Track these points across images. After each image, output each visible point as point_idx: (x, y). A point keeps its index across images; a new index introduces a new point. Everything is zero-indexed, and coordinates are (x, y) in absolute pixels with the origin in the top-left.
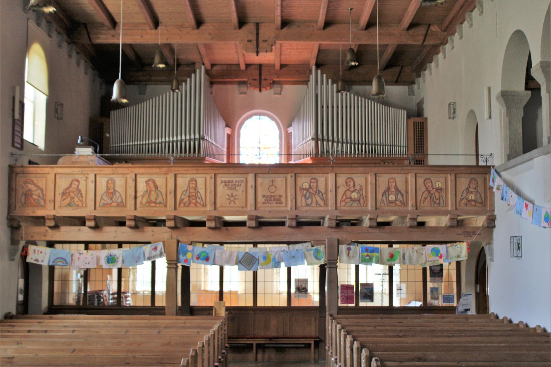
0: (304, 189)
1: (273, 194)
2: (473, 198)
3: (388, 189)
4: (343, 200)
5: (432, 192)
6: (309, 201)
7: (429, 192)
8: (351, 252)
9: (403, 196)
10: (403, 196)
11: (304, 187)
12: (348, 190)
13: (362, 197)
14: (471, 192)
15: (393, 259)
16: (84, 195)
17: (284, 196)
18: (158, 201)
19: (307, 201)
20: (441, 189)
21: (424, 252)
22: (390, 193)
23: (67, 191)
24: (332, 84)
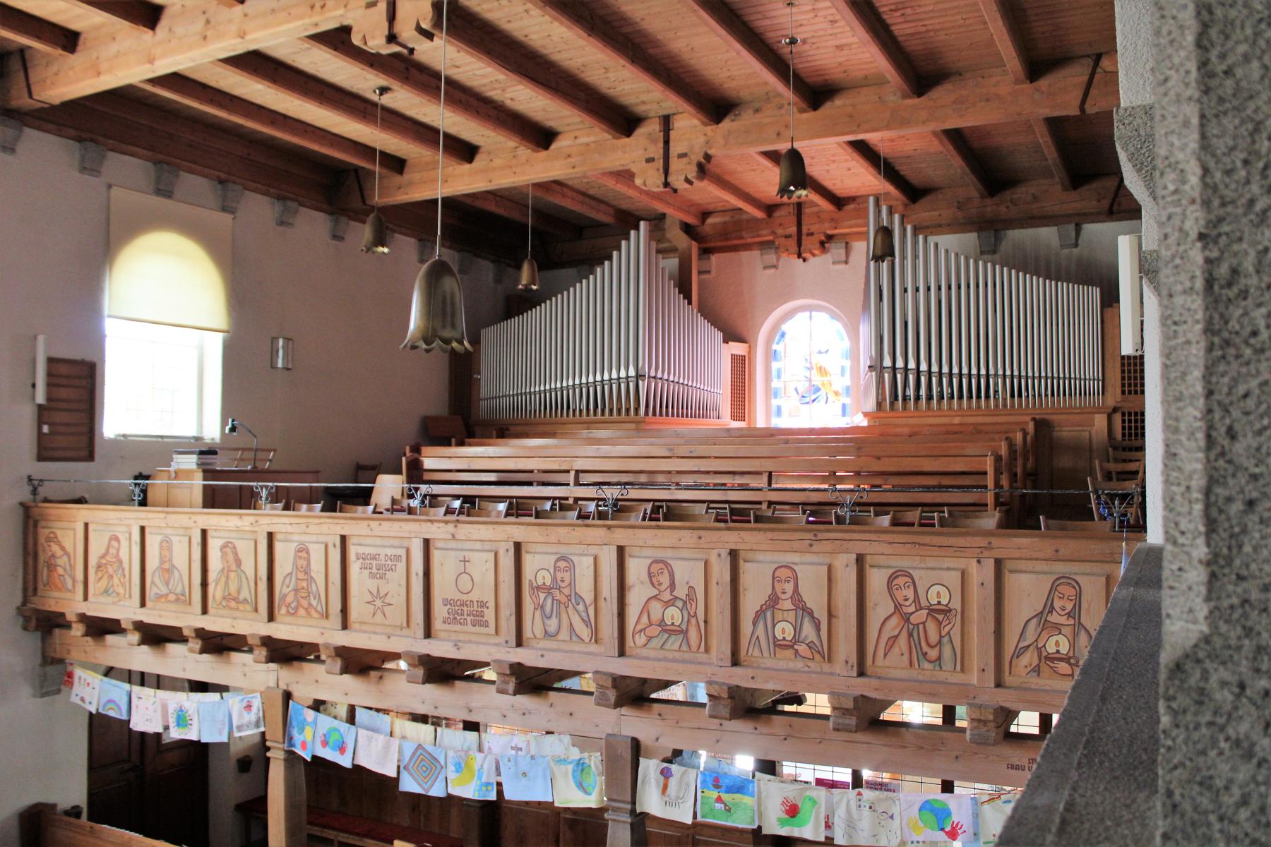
0: (538, 588)
1: (465, 597)
2: (1064, 649)
3: (773, 601)
4: (639, 627)
5: (913, 619)
6: (552, 624)
7: (906, 619)
8: (673, 782)
9: (818, 630)
10: (818, 630)
11: (540, 582)
12: (655, 597)
13: (693, 621)
14: (1057, 628)
15: (796, 820)
16: (127, 572)
17: (492, 604)
18: (241, 597)
19: (548, 622)
20: (947, 611)
21: (895, 810)
22: (779, 615)
23: (104, 561)
24: (915, 234)
